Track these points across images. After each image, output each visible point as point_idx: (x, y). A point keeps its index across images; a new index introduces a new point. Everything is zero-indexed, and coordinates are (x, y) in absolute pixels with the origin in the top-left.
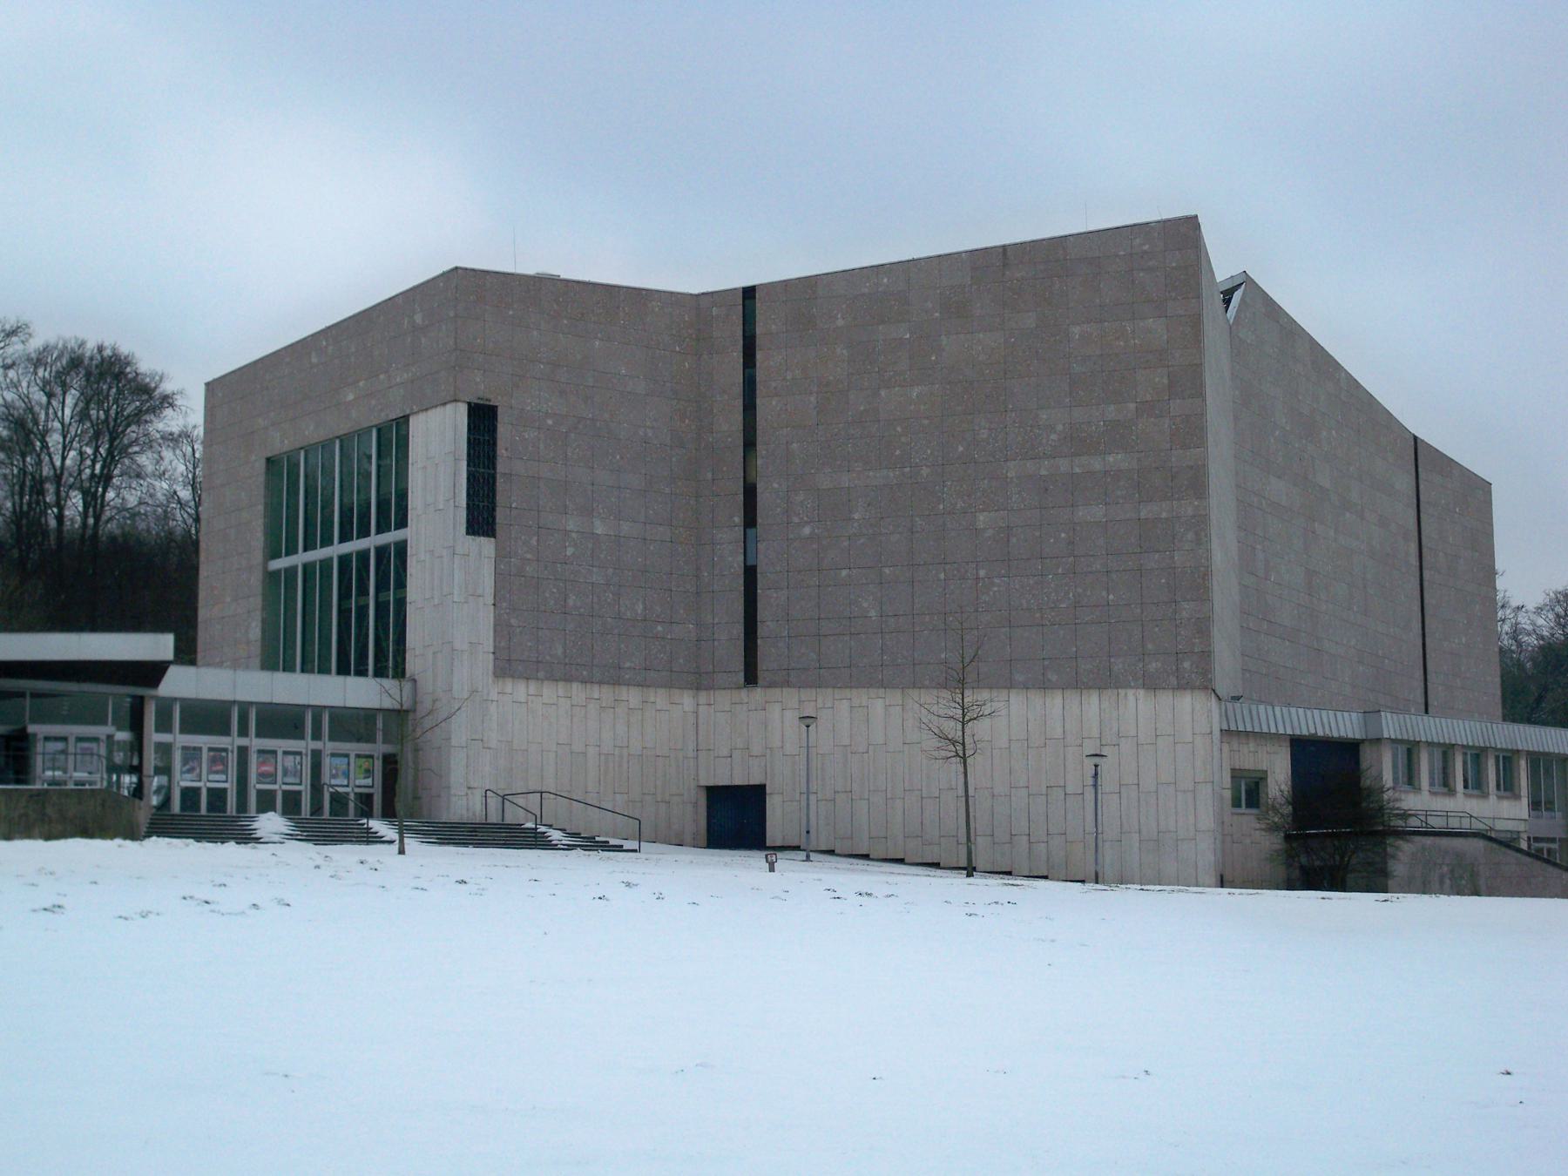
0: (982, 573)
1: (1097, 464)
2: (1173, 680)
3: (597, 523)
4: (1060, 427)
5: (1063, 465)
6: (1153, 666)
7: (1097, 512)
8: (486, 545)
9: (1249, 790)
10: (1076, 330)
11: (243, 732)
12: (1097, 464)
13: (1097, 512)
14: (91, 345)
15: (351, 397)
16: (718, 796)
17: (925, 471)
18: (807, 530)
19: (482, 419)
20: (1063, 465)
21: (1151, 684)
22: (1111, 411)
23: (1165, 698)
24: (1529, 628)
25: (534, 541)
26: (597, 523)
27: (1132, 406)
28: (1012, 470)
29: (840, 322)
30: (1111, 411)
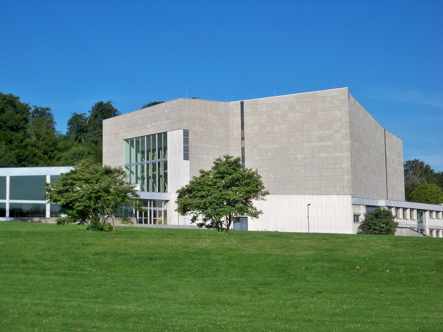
0: (298, 168)
1: (325, 144)
2: (343, 193)
3: (210, 156)
4: (316, 135)
5: (317, 144)
6: (338, 190)
7: (325, 155)
8: (188, 162)
9: (356, 217)
10: (320, 113)
11: (150, 206)
12: (325, 144)
13: (325, 155)
14: (432, 169)
15: (149, 126)
16: (239, 221)
17: (285, 145)
18: (257, 158)
19: (186, 133)
20: (317, 144)
21: (338, 194)
22: (328, 132)
23: (341, 197)
24: (241, 177)
25: (197, 161)
26: (210, 156)
27: (333, 131)
28: (305, 145)
29: (264, 110)
30: (328, 132)
